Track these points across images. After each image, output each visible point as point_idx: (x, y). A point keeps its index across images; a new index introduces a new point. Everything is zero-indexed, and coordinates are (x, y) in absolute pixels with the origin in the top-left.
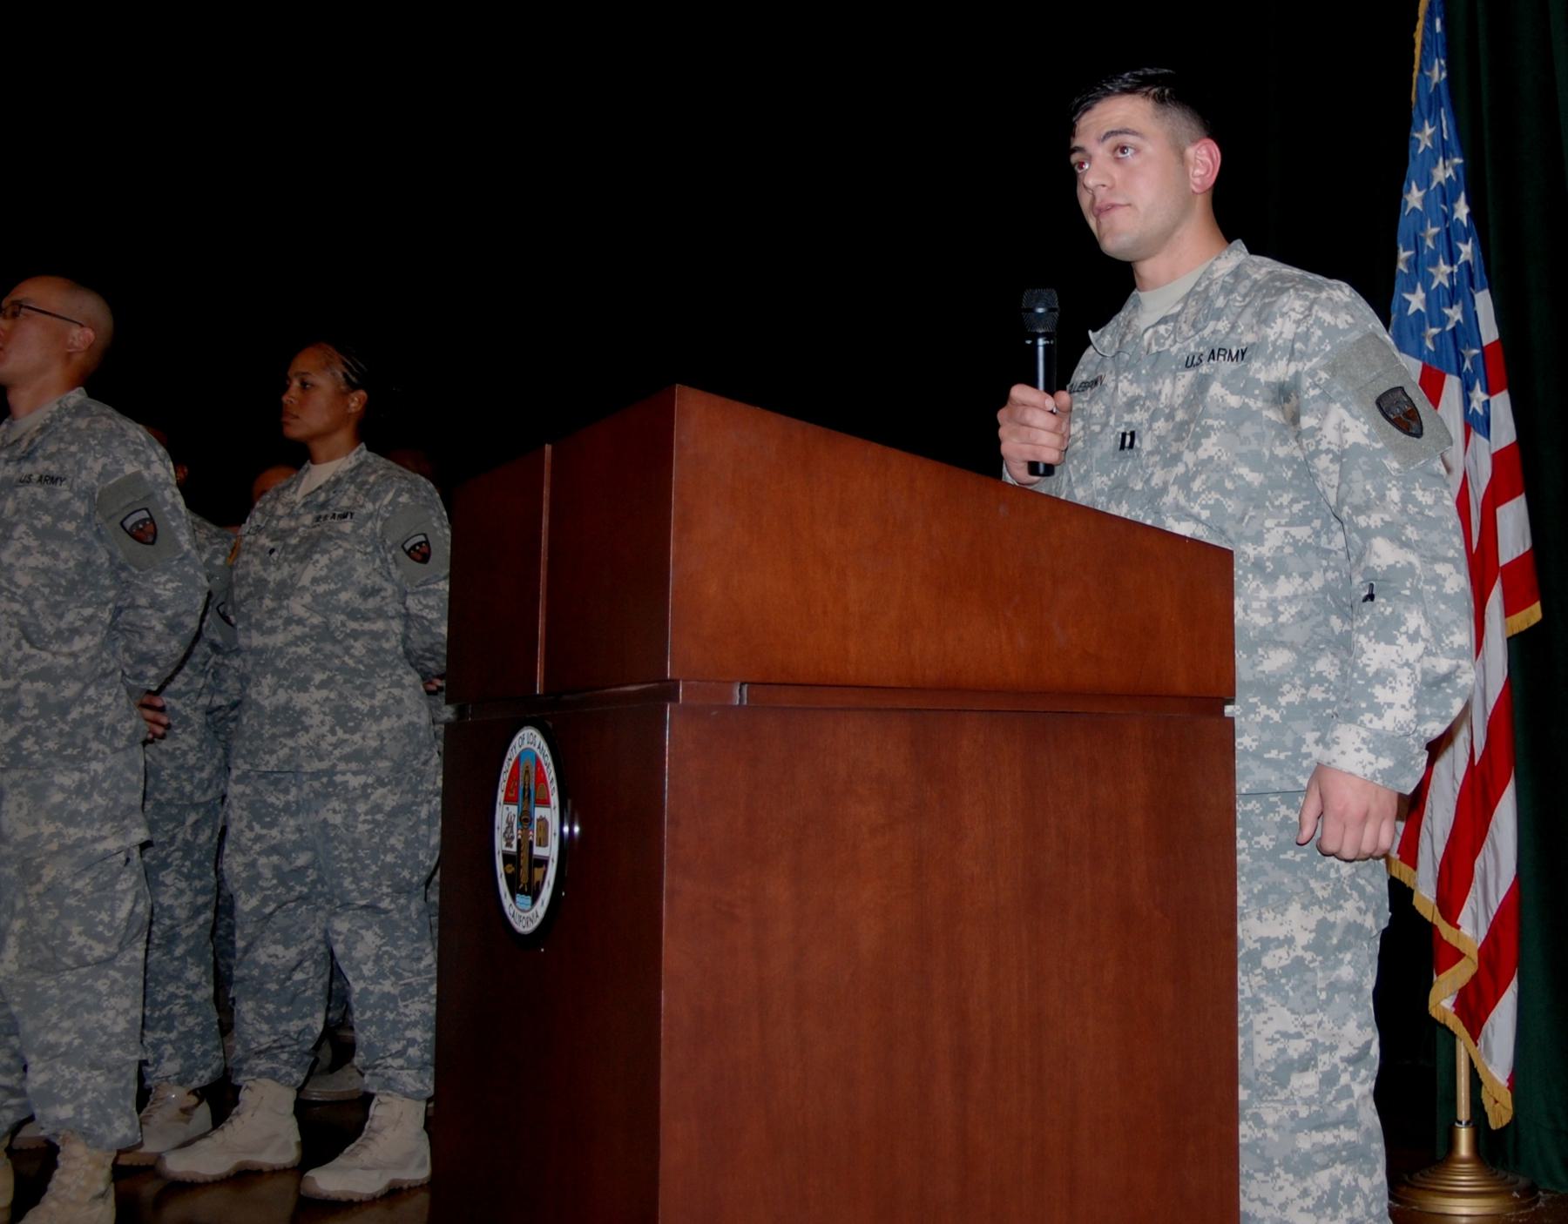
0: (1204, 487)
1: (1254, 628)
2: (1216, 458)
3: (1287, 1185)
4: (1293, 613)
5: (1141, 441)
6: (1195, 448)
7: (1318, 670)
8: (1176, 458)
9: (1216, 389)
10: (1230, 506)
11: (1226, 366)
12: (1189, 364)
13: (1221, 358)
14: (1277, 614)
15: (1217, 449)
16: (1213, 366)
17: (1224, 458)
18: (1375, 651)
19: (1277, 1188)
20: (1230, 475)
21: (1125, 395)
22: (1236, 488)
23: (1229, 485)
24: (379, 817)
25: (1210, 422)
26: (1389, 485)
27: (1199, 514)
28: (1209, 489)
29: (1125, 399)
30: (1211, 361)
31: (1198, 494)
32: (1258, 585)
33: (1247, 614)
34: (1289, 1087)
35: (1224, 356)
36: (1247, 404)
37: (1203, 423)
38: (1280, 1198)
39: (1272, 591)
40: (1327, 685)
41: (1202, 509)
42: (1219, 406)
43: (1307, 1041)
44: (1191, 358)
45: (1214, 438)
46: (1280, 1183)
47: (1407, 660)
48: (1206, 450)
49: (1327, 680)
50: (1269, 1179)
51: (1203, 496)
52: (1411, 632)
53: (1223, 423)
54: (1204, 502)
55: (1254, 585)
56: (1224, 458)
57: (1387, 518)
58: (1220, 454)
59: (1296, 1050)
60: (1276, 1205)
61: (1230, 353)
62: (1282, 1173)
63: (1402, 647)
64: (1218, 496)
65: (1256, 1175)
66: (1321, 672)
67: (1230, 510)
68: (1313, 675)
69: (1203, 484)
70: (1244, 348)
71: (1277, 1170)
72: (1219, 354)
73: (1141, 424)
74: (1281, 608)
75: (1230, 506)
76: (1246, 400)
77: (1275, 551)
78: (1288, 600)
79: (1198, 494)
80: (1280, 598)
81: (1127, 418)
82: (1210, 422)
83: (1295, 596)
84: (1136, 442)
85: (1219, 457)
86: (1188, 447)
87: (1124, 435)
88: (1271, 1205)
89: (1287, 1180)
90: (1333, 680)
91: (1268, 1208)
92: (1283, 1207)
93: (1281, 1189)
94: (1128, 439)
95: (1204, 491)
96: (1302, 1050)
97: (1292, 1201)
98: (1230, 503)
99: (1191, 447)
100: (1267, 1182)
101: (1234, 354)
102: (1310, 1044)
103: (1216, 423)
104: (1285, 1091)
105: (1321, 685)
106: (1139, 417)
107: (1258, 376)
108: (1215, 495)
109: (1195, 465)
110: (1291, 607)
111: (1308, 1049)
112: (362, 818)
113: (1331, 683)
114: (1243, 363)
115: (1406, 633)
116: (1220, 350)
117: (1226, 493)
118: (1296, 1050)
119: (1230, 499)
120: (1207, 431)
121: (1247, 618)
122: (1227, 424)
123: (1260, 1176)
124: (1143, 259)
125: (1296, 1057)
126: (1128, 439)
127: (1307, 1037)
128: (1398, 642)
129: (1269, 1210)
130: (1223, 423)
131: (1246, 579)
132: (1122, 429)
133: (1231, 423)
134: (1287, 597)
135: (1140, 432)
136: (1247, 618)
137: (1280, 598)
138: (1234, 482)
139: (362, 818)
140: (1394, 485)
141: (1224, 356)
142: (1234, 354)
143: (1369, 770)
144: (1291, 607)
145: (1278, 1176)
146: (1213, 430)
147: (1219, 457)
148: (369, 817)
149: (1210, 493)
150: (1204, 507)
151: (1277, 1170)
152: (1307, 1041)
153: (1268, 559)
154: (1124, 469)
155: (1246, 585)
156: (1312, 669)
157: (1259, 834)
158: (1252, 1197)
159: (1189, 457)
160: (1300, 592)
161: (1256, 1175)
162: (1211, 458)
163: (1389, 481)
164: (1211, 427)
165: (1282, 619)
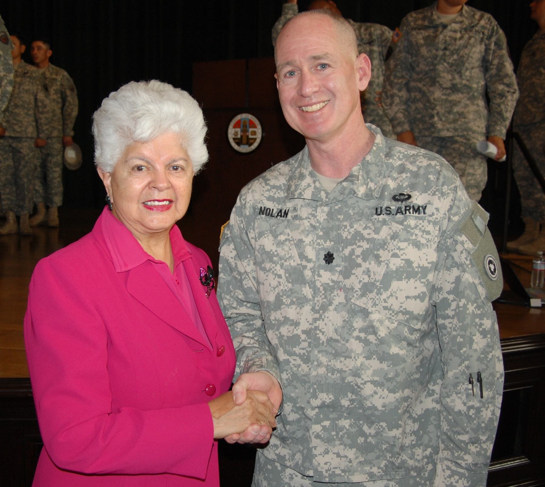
3: (322, 465)
7: (485, 340)
19: (329, 464)
24: (372, 338)
34: (390, 290)
38: (327, 458)
43: (402, 260)
46: (326, 467)
50: (332, 470)
59: (394, 264)
60: (330, 453)
62: (324, 473)
65: (340, 472)
71: (327, 475)
88: (334, 453)
89: (323, 468)
91: (336, 451)
92: (327, 452)
93: (326, 463)
96: (398, 265)
97: (321, 454)
98: (406, 334)
100: (334, 468)
102: (404, 262)
104: (387, 292)
105: (484, 329)
111: (402, 265)
112: (356, 333)
118: (394, 264)
123: (338, 472)
124: (532, 298)
125: (394, 269)
127: (402, 257)
129: (335, 451)
139: (356, 333)
143: (408, 221)
145: (327, 471)
148: (362, 335)
151: (327, 475)
152: (402, 260)
156: (489, 340)
157: (477, 452)
158: (345, 459)
161: (340, 472)
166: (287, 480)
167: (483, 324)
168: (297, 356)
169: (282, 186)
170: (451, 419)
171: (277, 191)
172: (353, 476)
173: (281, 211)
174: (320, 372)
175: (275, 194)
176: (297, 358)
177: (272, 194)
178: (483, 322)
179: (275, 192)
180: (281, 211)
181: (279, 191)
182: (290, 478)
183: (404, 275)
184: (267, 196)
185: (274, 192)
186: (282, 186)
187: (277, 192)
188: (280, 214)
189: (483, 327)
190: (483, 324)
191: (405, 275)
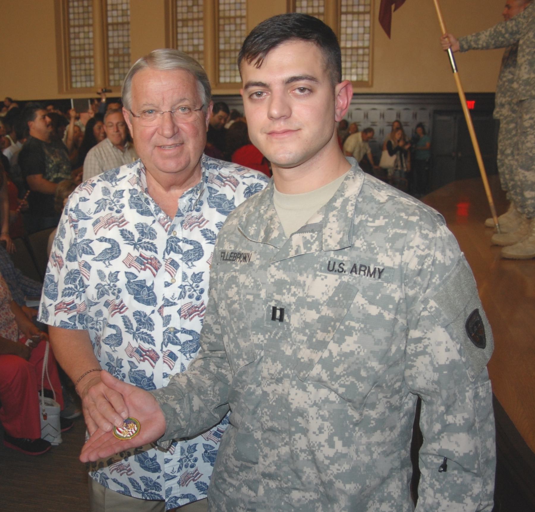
0: (345, 372)
1: (363, 464)
2: (356, 353)
4: (379, 452)
5: (289, 317)
6: (340, 341)
7: (389, 490)
8: (323, 345)
9: (359, 300)
10: (361, 387)
11: (368, 280)
12: (331, 268)
13: (362, 273)
14: (371, 453)
15: (356, 346)
16: (355, 278)
17: (362, 353)
18: (296, 394)
20: (365, 367)
21: (273, 277)
22: (368, 376)
23: (363, 373)
25: (353, 324)
26: (468, 389)
27: (337, 389)
28: (348, 375)
29: (273, 280)
30: (354, 274)
31: (339, 377)
32: (361, 434)
33: (358, 456)
35: (364, 271)
36: (382, 314)
37: (347, 323)
39: (369, 438)
40: (393, 502)
41: (340, 386)
42: (359, 312)
44: (332, 263)
45: (355, 337)
47: (315, 401)
48: (348, 345)
49: (393, 499)
51: (343, 378)
52: (474, 496)
53: (362, 326)
54: (342, 383)
55: (358, 434)
56: (362, 353)
57: (466, 416)
58: (359, 350)
61: (369, 271)
63: (467, 505)
64: (354, 380)
66: (390, 492)
67: (360, 390)
68: (385, 494)
69: (344, 370)
70: (381, 268)
72: (360, 270)
73: (290, 305)
74: (373, 449)
75: (361, 387)
76: (382, 311)
77: (381, 415)
78: (379, 444)
79: (339, 377)
80: (373, 442)
81: (277, 297)
82: (353, 324)
83: (384, 443)
84: (286, 317)
85: (358, 353)
86: (333, 339)
87: (274, 309)
90: (396, 498)
94: (278, 313)
95: (344, 376)
98: (361, 385)
99: (336, 340)
101: (372, 270)
103: (357, 325)
105: (390, 502)
106: (287, 299)
107: (393, 295)
108: (351, 379)
109: (338, 355)
110: (378, 448)
113: (395, 501)
114: (380, 281)
115: (471, 496)
116: (361, 266)
117: (361, 379)
119: (362, 383)
120: (349, 331)
121: (359, 459)
122: (365, 326)
126: (278, 313)
128: (464, 501)
130: (362, 326)
131: (355, 431)
132: (273, 304)
133: (368, 326)
134: (378, 442)
135: (289, 310)
136: (359, 459)
137: (373, 442)
138: (368, 372)
140: (470, 388)
141: (364, 271)
142: (372, 270)
144: (378, 448)
146: (356, 331)
147: (358, 353)
149: (348, 377)
150: (341, 386)
153: (374, 419)
154: (276, 334)
155: (354, 434)
159: (333, 347)
160: (387, 440)
162: (352, 353)
163: (468, 386)
164: (354, 328)
165: (375, 456)
166: (327, 424)
167: (390, 506)
168: (214, 333)
169: (415, 359)
170: (380, 315)
171: (415, 351)
172: (155, 240)
173: (355, 266)
174: (344, 280)
175: (416, 348)
176: (215, 331)
177: (419, 345)
178: (390, 509)
179: (416, 349)
180: (355, 266)
181: (413, 352)
182: (323, 428)
183: (378, 295)
184: (423, 341)
185: (418, 348)
186: (415, 359)
187: (414, 349)
188: (354, 270)
189: (390, 504)
190: (390, 506)
191: (378, 298)
